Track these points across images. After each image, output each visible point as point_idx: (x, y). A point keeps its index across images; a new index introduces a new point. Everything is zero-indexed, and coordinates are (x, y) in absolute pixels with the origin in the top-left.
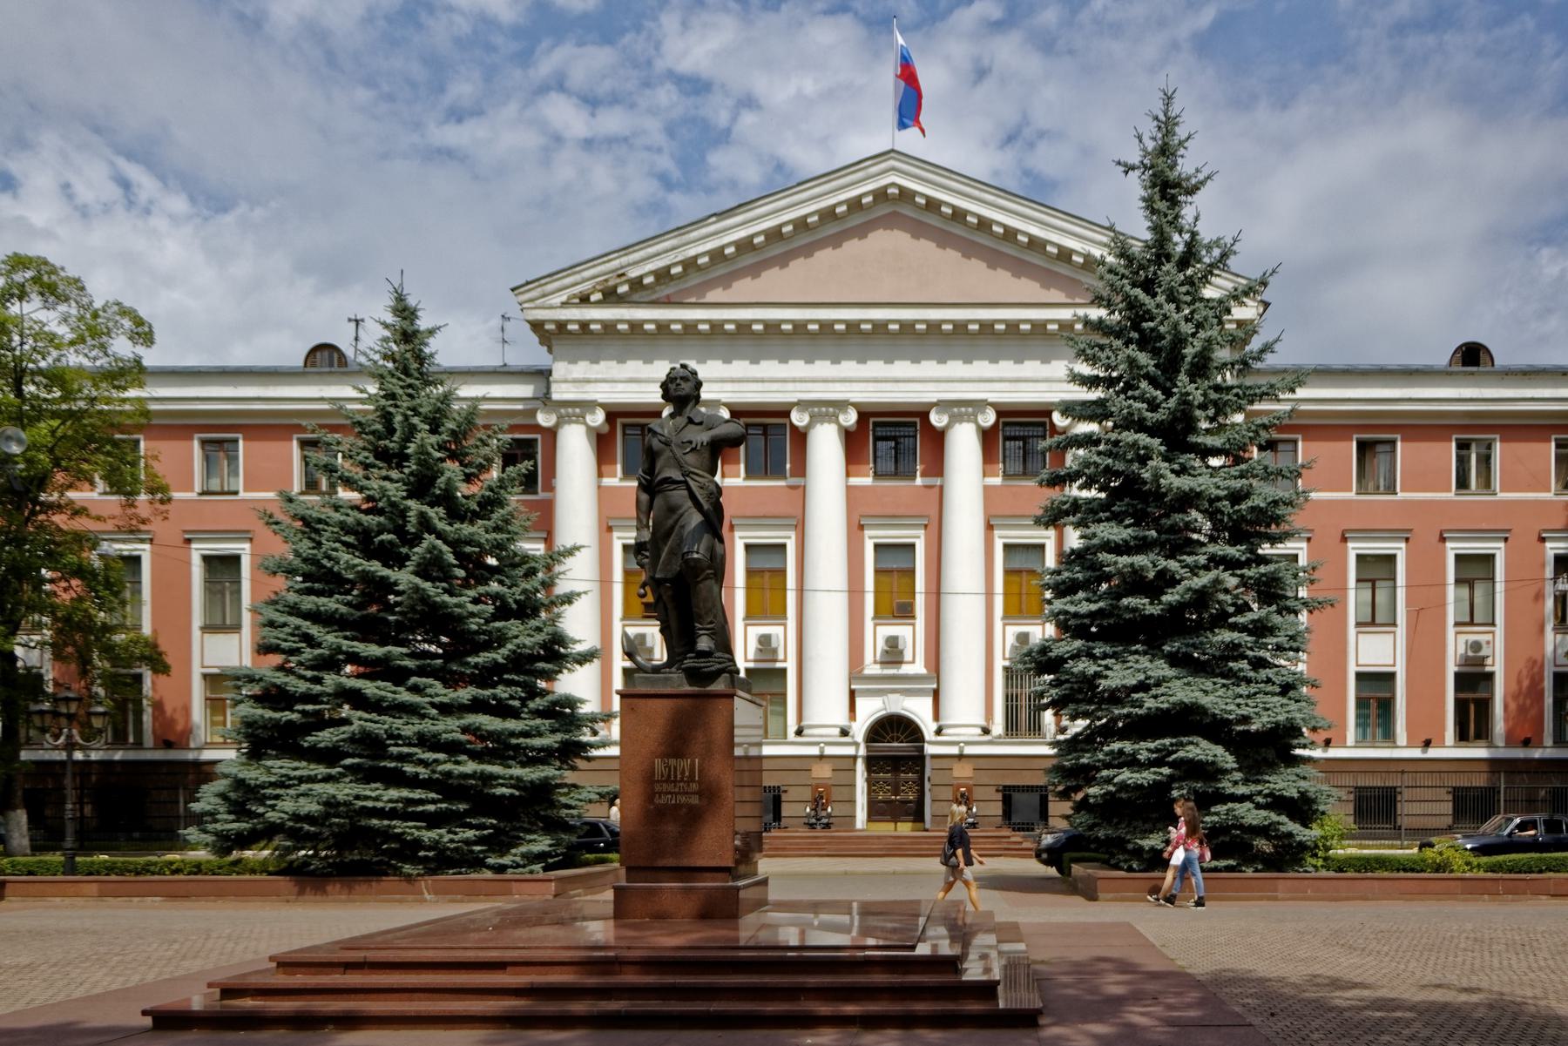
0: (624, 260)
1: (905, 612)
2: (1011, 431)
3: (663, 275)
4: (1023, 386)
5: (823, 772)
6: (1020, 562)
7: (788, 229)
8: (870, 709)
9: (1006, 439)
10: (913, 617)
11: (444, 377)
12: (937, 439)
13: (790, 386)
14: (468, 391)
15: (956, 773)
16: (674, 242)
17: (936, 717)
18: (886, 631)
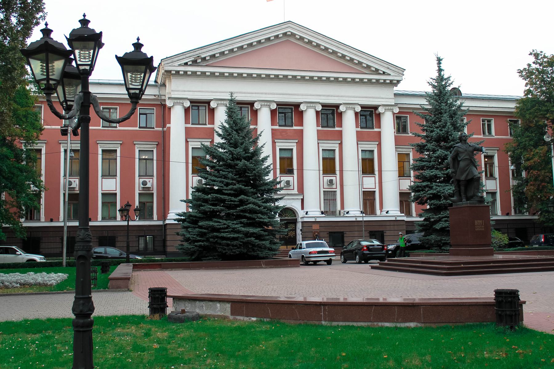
0: (200, 51)
1: (372, 172)
2: (281, 111)
3: (213, 56)
4: (330, 98)
9: (279, 113)
10: (293, 174)
12: (301, 114)
13: (254, 95)
14: (467, 103)
16: (217, 46)
17: (303, 208)
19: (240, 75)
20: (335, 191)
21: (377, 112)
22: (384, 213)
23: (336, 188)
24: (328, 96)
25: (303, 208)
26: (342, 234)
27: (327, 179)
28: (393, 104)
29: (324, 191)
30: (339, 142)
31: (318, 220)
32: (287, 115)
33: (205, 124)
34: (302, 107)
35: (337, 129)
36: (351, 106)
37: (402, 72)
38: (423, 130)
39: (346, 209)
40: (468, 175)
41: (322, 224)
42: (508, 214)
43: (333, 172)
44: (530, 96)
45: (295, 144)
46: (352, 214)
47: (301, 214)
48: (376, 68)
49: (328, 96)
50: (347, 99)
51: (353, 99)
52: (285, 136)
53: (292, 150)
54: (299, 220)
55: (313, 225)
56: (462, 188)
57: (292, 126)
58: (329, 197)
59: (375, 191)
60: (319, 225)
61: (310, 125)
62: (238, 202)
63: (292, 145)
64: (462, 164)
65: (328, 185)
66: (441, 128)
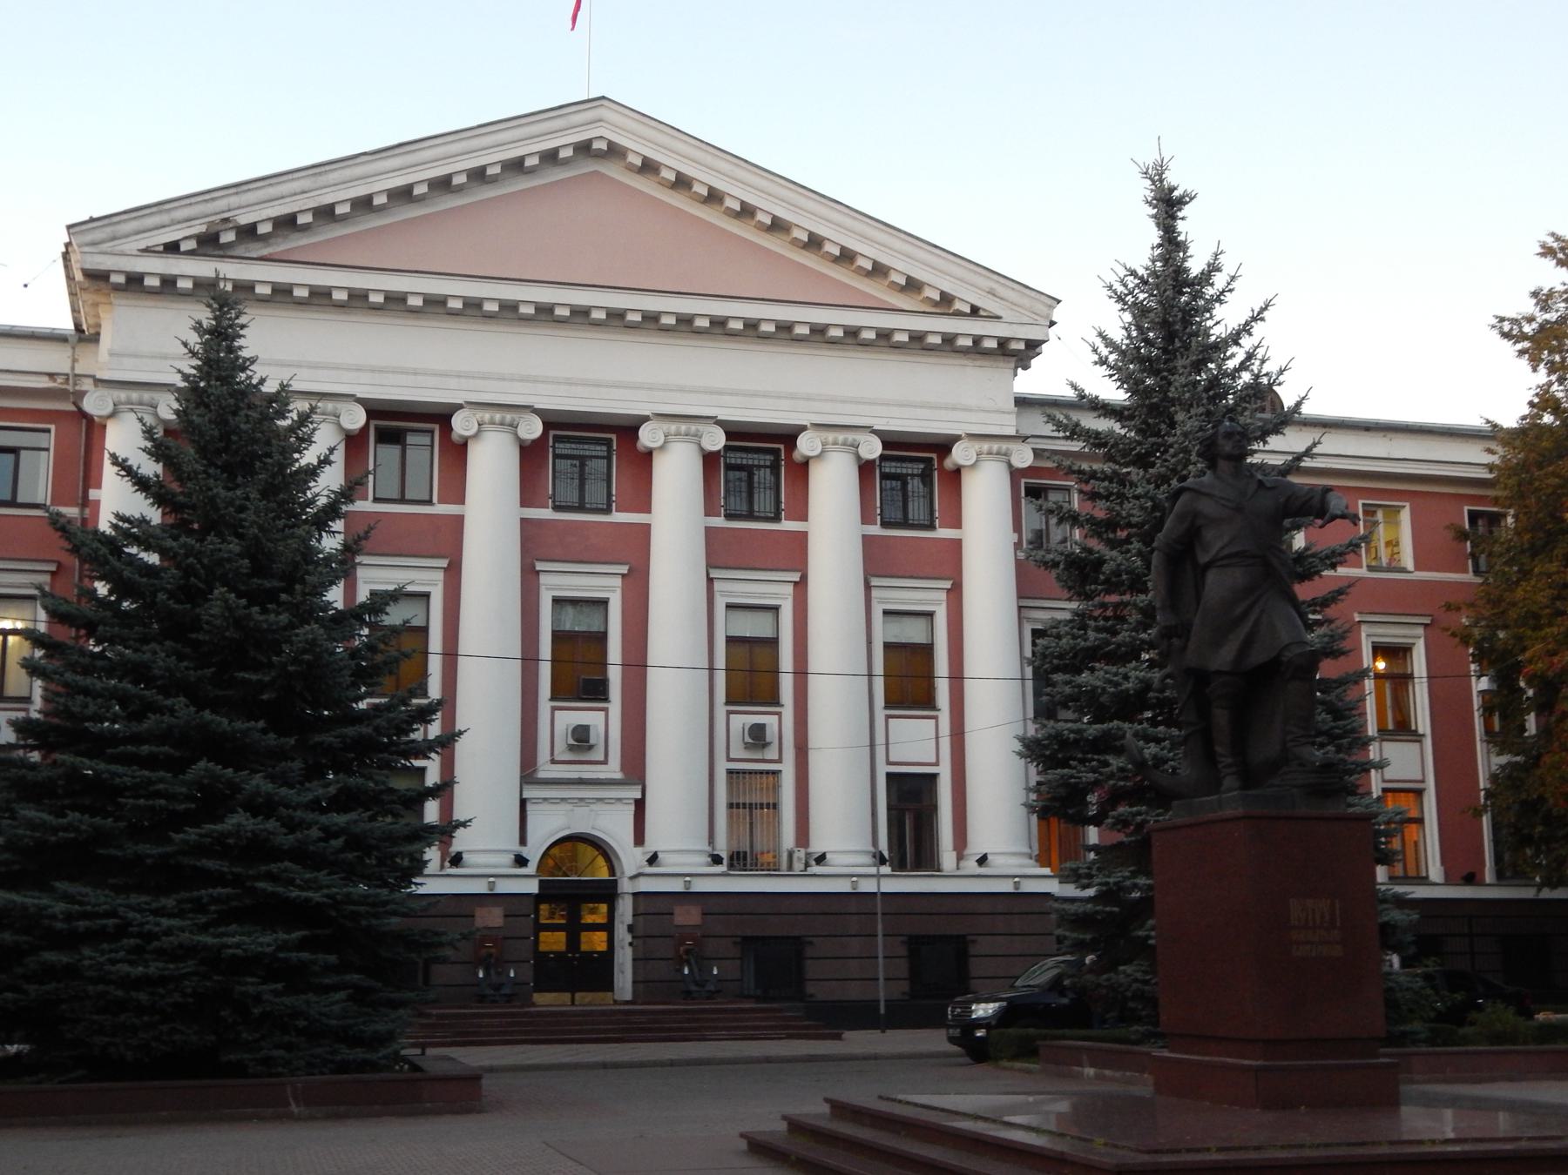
0: (234, 201)
1: (595, 691)
5: (492, 918)
6: (573, 621)
8: (548, 825)
9: (556, 456)
10: (606, 700)
13: (453, 383)
17: (639, 839)
19: (396, 301)
20: (776, 773)
21: (948, 464)
22: (971, 866)
23: (779, 761)
25: (639, 839)
26: (797, 945)
27: (742, 721)
28: (1013, 433)
30: (796, 577)
31: (700, 886)
32: (592, 465)
33: (429, 502)
34: (648, 437)
35: (787, 525)
38: (1093, 496)
39: (817, 847)
40: (1247, 644)
42: (1471, 879)
43: (595, 691)
44: (1548, 419)
45: (618, 581)
46: (837, 863)
47: (630, 859)
49: (755, 395)
53: (604, 603)
54: (626, 886)
55: (677, 910)
56: (1221, 717)
57: (608, 511)
59: (934, 776)
62: (189, 798)
64: (1218, 584)
65: (747, 746)
66: (1182, 493)
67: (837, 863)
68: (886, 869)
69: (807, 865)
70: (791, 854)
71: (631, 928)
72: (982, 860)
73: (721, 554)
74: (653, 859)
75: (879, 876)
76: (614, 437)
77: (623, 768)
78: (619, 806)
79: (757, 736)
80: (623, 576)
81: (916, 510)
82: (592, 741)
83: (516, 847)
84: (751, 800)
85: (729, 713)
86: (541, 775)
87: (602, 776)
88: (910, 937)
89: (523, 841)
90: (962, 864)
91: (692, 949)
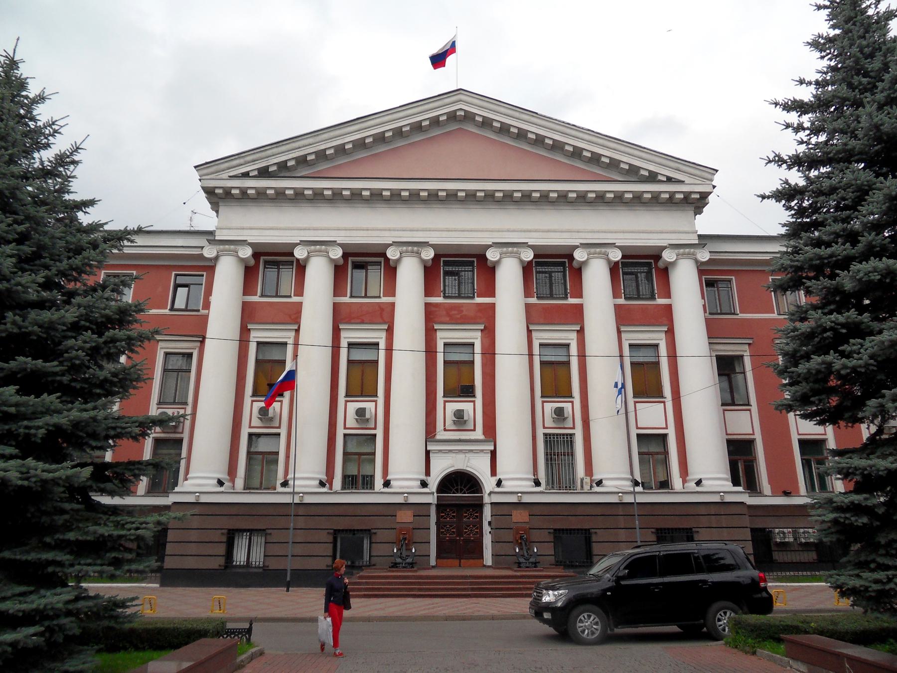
1: (467, 391)
5: (406, 517)
7: (349, 146)
8: (442, 466)
11: (597, 531)
13: (387, 233)
15: (514, 519)
16: (311, 141)
17: (494, 472)
18: (452, 407)
21: (661, 264)
22: (691, 486)
23: (574, 428)
24: (548, 231)
25: (494, 472)
26: (586, 535)
29: (545, 435)
31: (527, 499)
33: (379, 297)
35: (572, 301)
36: (598, 250)
37: (709, 176)
41: (536, 510)
45: (479, 334)
46: (610, 485)
47: (488, 483)
48: (650, 172)
49: (548, 231)
50: (589, 235)
51: (506, 234)
52: (458, 317)
54: (487, 499)
57: (566, 298)
58: (652, 446)
60: (399, 519)
61: (509, 293)
63: (658, 337)
67: (610, 485)
68: (639, 489)
69: (591, 487)
70: (582, 480)
71: (490, 523)
72: (699, 483)
73: (534, 317)
74: (499, 483)
75: (634, 493)
76: (475, 260)
77: (484, 433)
78: (482, 455)
79: (559, 413)
80: (482, 330)
81: (644, 289)
82: (465, 418)
83: (423, 477)
84: (557, 452)
85: (543, 402)
86: (438, 437)
87: (473, 438)
88: (657, 529)
89: (428, 473)
90: (686, 485)
91: (523, 539)
